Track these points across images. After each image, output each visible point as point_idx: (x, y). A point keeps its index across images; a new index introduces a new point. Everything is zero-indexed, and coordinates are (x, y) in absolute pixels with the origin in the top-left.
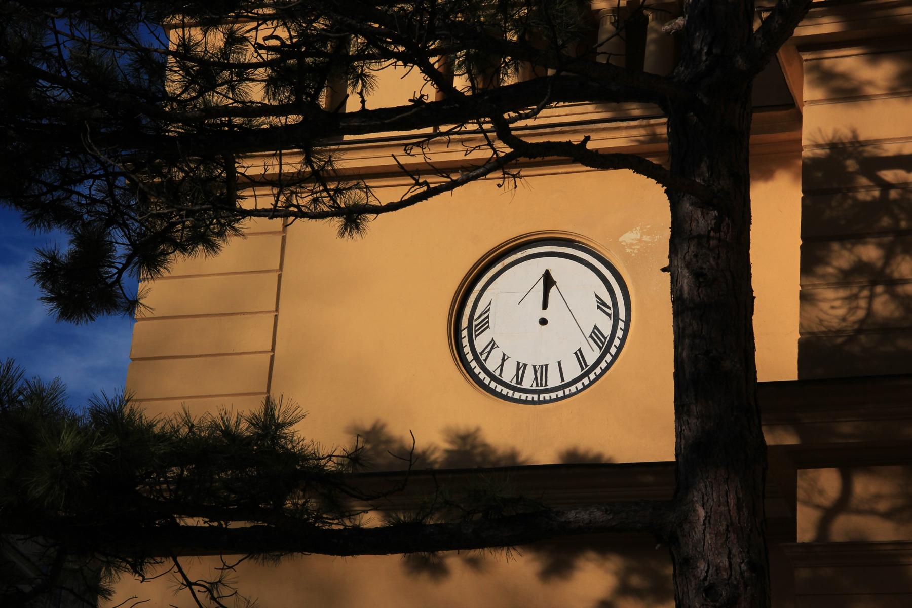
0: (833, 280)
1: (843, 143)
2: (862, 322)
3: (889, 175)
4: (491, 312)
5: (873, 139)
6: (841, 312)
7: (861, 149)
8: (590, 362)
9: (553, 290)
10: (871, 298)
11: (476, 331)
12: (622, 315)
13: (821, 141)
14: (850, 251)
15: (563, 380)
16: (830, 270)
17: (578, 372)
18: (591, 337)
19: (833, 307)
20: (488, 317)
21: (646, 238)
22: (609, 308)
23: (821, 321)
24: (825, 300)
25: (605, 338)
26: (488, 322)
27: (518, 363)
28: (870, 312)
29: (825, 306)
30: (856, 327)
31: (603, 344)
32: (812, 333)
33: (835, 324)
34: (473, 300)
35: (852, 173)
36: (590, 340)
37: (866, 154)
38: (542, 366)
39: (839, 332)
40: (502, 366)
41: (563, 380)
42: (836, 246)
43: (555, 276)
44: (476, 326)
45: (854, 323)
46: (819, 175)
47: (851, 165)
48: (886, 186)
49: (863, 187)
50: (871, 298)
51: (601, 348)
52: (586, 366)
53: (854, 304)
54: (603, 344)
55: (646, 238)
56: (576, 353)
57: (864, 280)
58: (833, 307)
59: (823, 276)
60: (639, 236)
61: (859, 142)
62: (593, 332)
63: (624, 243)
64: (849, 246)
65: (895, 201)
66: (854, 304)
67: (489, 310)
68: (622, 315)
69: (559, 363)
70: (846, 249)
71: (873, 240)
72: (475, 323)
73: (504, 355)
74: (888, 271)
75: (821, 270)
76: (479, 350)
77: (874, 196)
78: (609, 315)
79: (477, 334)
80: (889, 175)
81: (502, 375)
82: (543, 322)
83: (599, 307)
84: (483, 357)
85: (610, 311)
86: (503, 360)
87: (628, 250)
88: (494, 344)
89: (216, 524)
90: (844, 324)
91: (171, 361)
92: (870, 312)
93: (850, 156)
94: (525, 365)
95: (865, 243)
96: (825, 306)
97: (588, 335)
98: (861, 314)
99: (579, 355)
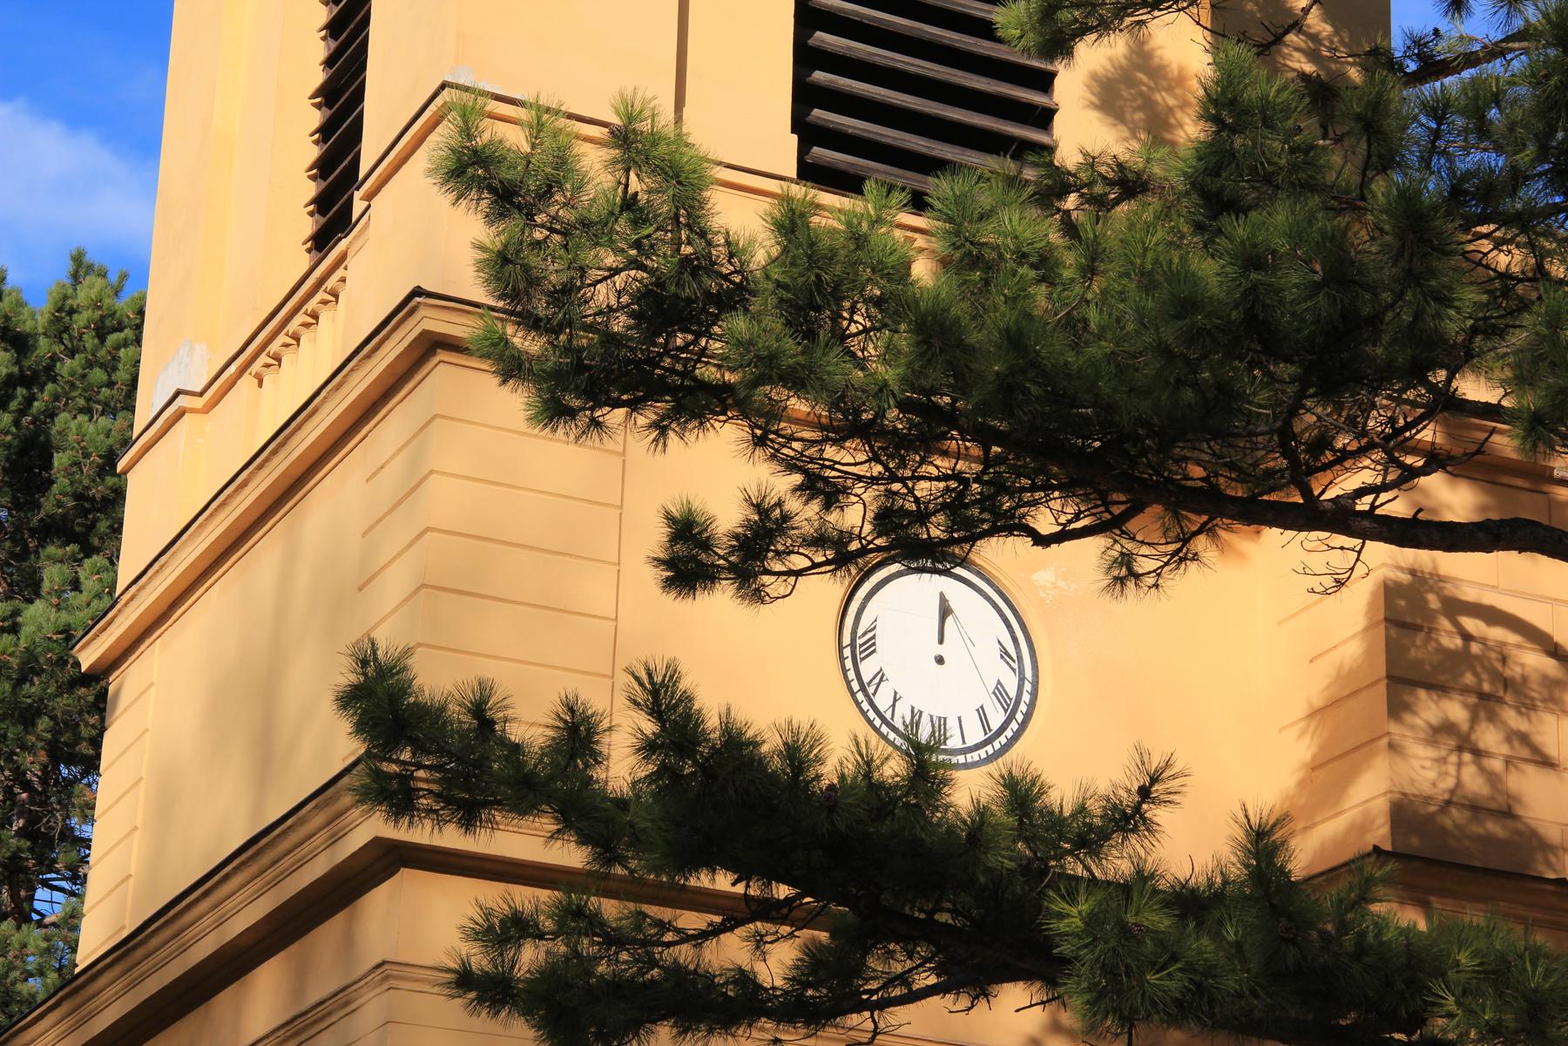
0: (1423, 735)
1: (1422, 572)
2: (1453, 792)
3: (1471, 624)
4: (877, 631)
5: (1452, 575)
6: (1432, 775)
7: (1441, 584)
8: (995, 726)
9: (949, 620)
10: (1460, 765)
11: (861, 653)
12: (1029, 674)
13: (1403, 564)
14: (1437, 703)
15: (964, 742)
16: (1418, 721)
17: (981, 737)
18: (994, 693)
19: (1423, 767)
20: (874, 637)
21: (1061, 583)
22: (1014, 661)
23: (1412, 781)
24: (1415, 757)
25: (1011, 700)
26: (874, 644)
27: (913, 708)
28: (1459, 784)
29: (1416, 764)
30: (1446, 796)
31: (1008, 705)
32: (1404, 794)
33: (1426, 788)
34: (856, 610)
35: (1435, 611)
36: (993, 696)
37: (1446, 593)
38: (940, 718)
39: (1428, 799)
40: (894, 706)
41: (964, 742)
42: (1422, 693)
43: (953, 604)
44: (861, 646)
45: (1445, 791)
46: (1403, 603)
47: (1433, 602)
48: (1467, 637)
49: (1445, 631)
50: (1460, 765)
51: (1006, 711)
52: (990, 730)
53: (1443, 769)
54: (1008, 705)
55: (1061, 583)
56: (978, 710)
57: (1452, 743)
58: (1423, 767)
59: (1413, 727)
60: (1053, 579)
61: (1438, 576)
62: (997, 688)
63: (1037, 584)
64: (1435, 697)
65: (1477, 657)
66: (1443, 769)
67: (875, 627)
68: (1029, 674)
69: (960, 719)
70: (1432, 700)
71: (1460, 698)
72: (859, 642)
73: (896, 693)
74: (1473, 737)
75: (1408, 718)
76: (866, 680)
77: (1456, 645)
78: (1014, 670)
79: (862, 656)
80: (1471, 624)
81: (895, 719)
82: (940, 660)
83: (1002, 657)
84: (871, 690)
85: (1015, 666)
86: (895, 700)
87: (1043, 595)
88: (883, 675)
89: (754, 891)
90: (1435, 791)
91: (487, 601)
92: (1459, 784)
93: (1431, 590)
94: (921, 713)
95: (1451, 699)
96: (1416, 764)
97: (991, 692)
98: (1450, 783)
99: (981, 712)
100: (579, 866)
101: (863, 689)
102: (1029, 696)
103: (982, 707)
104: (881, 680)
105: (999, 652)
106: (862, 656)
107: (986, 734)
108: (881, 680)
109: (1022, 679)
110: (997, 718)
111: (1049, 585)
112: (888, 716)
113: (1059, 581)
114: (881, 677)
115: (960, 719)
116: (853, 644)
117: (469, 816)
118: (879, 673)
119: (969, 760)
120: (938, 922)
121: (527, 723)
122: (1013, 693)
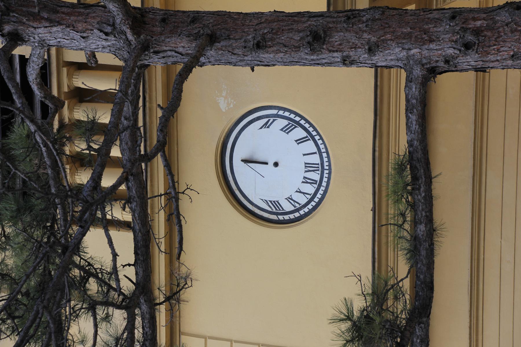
8: (305, 134)
11: (280, 210)
12: (274, 112)
15: (315, 153)
17: (311, 142)
20: (271, 201)
21: (224, 94)
22: (269, 120)
26: (274, 202)
27: (303, 182)
31: (293, 125)
38: (306, 166)
40: (304, 193)
41: (315, 153)
51: (296, 127)
52: (307, 137)
54: (293, 125)
60: (223, 99)
62: (285, 131)
67: (266, 200)
68: (274, 112)
69: (304, 155)
72: (274, 210)
73: (297, 191)
76: (293, 208)
78: (274, 121)
79: (281, 209)
86: (300, 192)
87: (232, 106)
94: (305, 178)
99: (299, 141)
100: (368, 7)
101: (297, 210)
102: (286, 112)
103: (296, 141)
104: (292, 199)
105: (266, 129)
106: (281, 209)
107: (309, 140)
108: (292, 199)
109: (278, 116)
110: (299, 133)
111: (226, 101)
112: (309, 197)
113: (223, 95)
114: (290, 199)
115: (304, 155)
116: (277, 214)
117: (139, 129)
118: (288, 200)
119: (327, 168)
120: (400, 341)
121: (112, 214)
122: (286, 122)
